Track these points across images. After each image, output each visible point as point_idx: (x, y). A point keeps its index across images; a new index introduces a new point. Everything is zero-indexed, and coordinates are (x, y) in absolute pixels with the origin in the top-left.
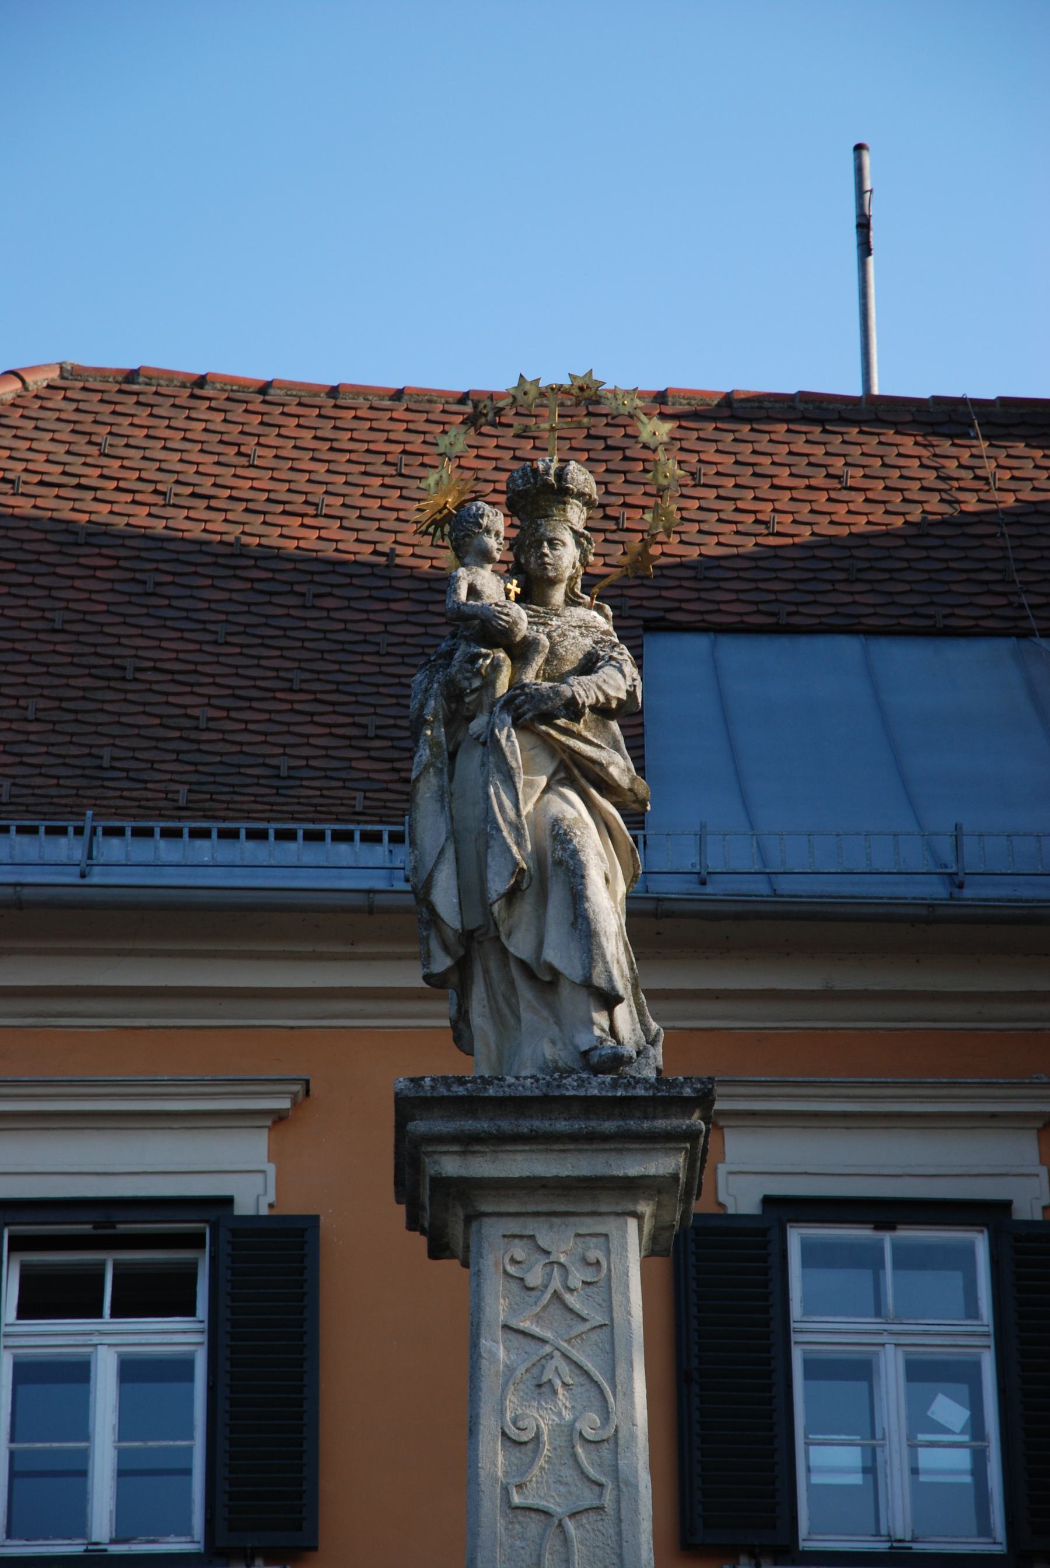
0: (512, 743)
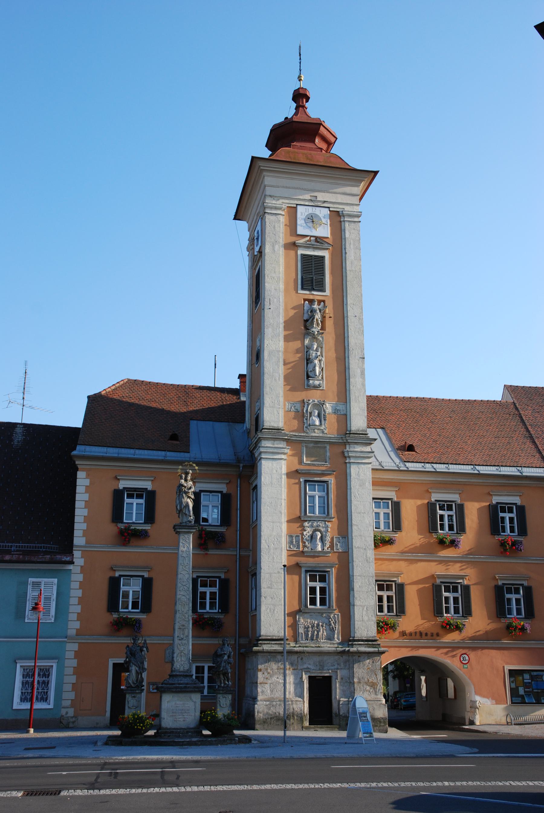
0: (184, 495)
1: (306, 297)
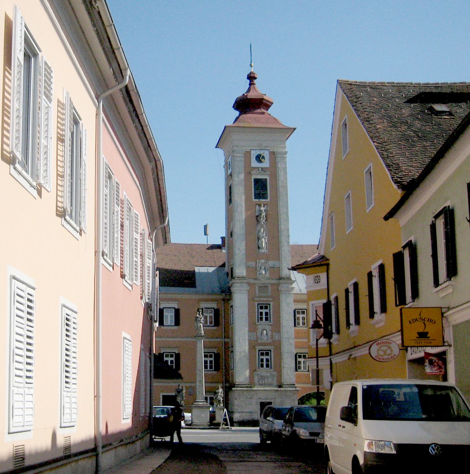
1: (257, 203)
